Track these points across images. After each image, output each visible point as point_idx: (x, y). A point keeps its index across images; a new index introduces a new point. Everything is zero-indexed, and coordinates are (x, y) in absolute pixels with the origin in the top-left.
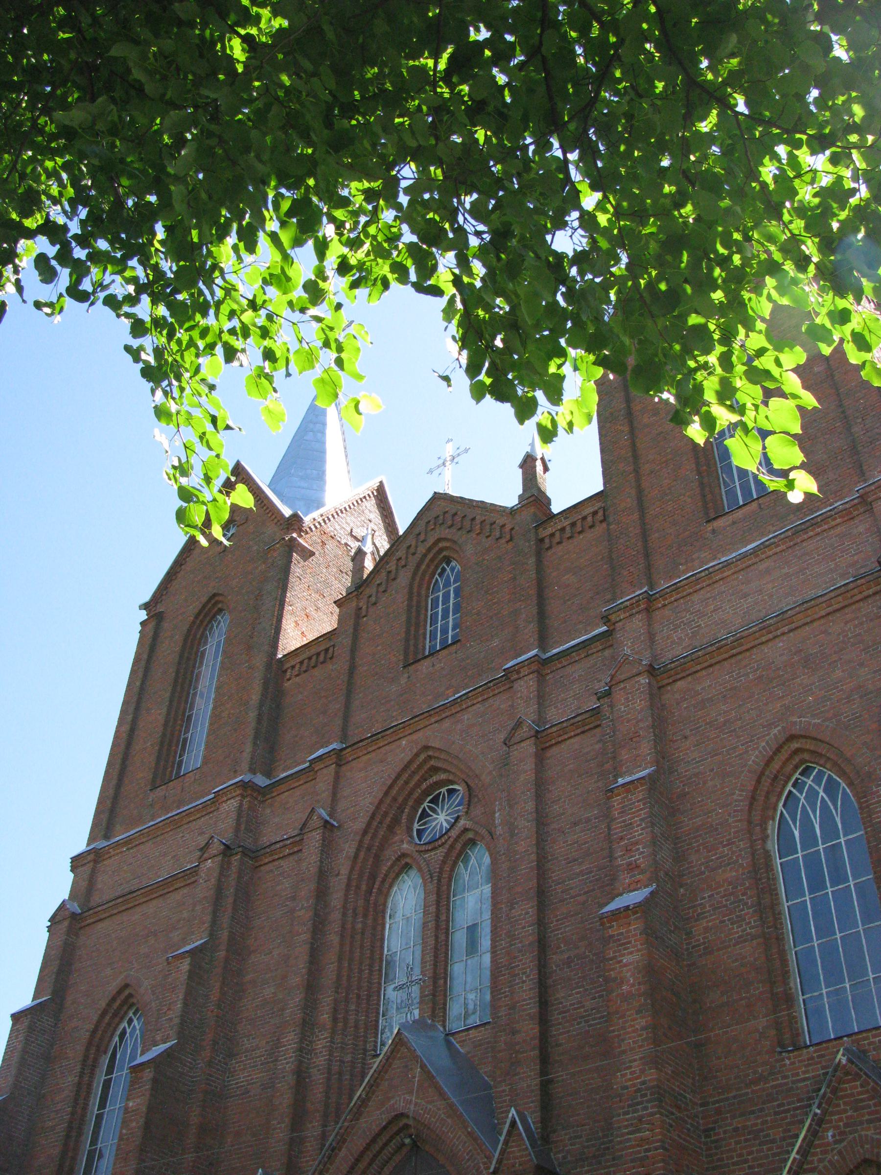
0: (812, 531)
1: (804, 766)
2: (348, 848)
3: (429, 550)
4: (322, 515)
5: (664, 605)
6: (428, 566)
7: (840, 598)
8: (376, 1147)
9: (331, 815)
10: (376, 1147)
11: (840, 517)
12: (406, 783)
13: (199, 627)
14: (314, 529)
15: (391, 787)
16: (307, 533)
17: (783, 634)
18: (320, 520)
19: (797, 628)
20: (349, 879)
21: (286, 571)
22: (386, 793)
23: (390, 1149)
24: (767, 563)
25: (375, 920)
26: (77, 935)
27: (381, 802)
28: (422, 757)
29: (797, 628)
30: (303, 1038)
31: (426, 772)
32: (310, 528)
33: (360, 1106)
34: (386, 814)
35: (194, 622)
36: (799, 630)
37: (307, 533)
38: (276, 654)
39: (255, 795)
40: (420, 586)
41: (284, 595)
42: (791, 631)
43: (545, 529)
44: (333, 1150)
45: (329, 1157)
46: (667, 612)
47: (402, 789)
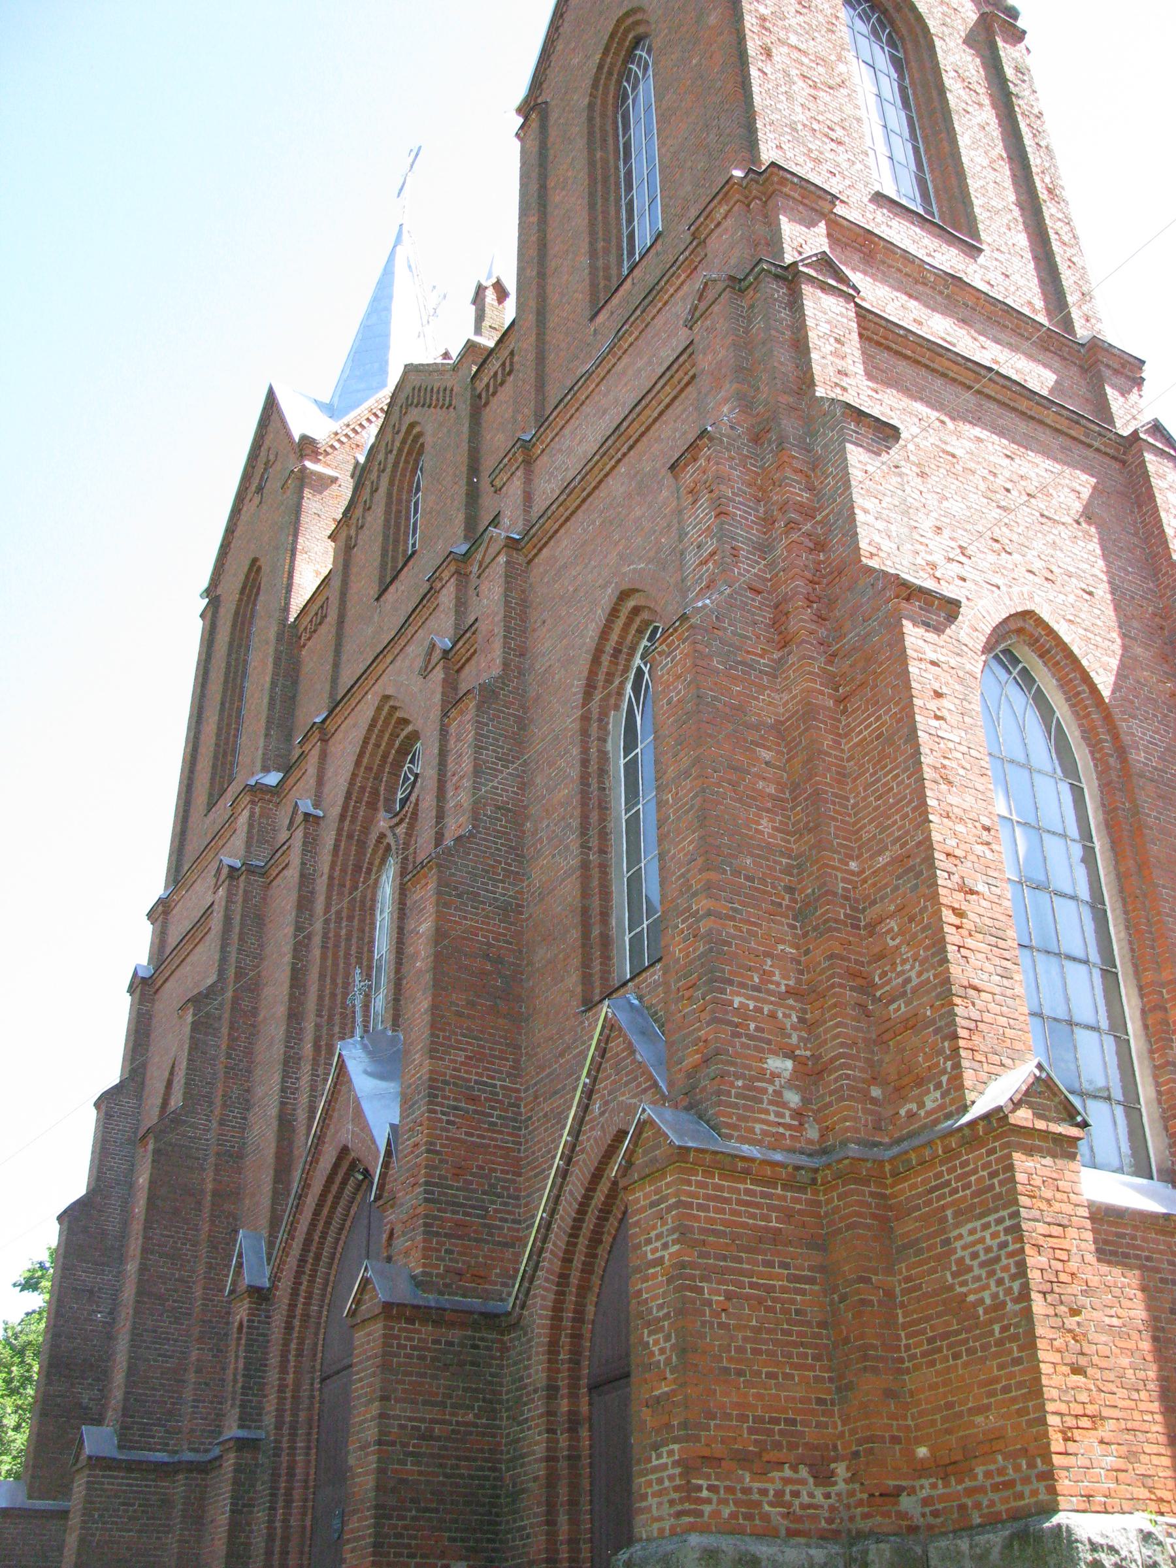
0: (660, 301)
1: (651, 628)
2: (328, 838)
3: (404, 442)
4: (348, 425)
5: (543, 451)
6: (407, 462)
7: (667, 388)
8: (334, 1188)
9: (316, 805)
10: (334, 1188)
11: (684, 272)
12: (377, 746)
13: (247, 605)
14: (337, 445)
15: (361, 755)
16: (327, 453)
17: (624, 455)
18: (348, 431)
19: (637, 441)
20: (331, 878)
21: (297, 510)
22: (358, 763)
23: (349, 1188)
24: (625, 360)
25: (362, 920)
26: (152, 1001)
27: (354, 776)
28: (386, 708)
29: (637, 441)
30: (285, 1076)
31: (395, 727)
32: (332, 447)
33: (318, 1144)
34: (363, 789)
35: (240, 600)
36: (639, 445)
37: (327, 453)
38: (287, 619)
39: (267, 797)
40: (400, 490)
41: (295, 542)
42: (631, 448)
43: (481, 380)
44: (300, 1199)
45: (297, 1207)
46: (545, 458)
47: (372, 755)
